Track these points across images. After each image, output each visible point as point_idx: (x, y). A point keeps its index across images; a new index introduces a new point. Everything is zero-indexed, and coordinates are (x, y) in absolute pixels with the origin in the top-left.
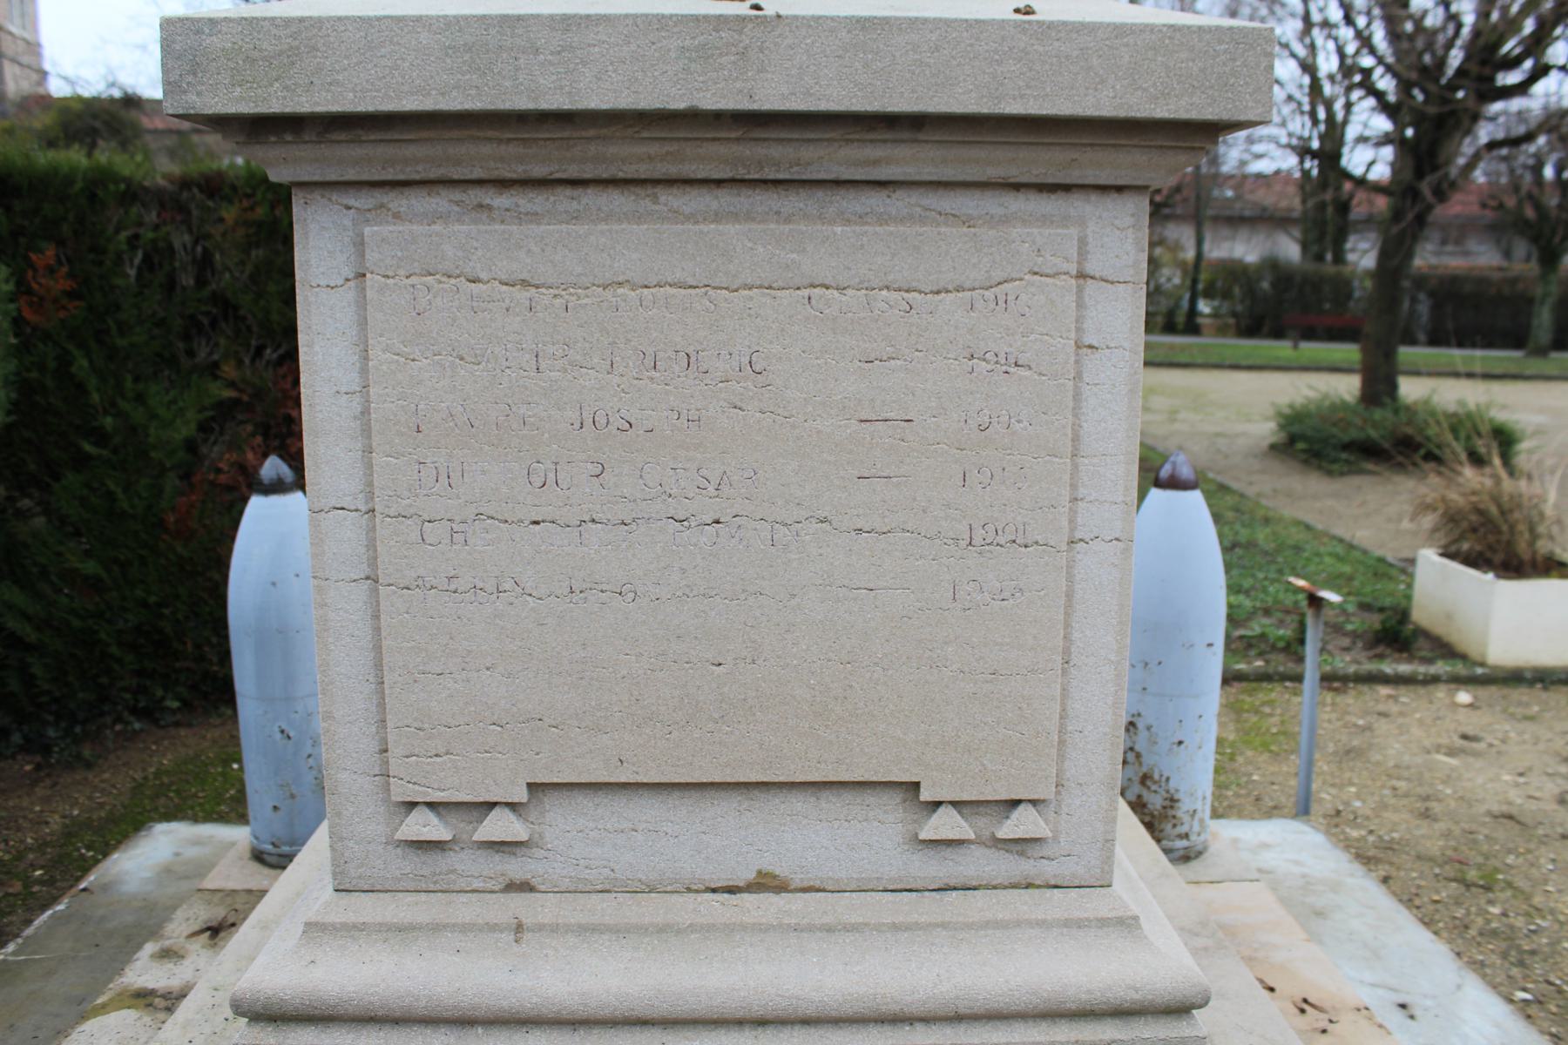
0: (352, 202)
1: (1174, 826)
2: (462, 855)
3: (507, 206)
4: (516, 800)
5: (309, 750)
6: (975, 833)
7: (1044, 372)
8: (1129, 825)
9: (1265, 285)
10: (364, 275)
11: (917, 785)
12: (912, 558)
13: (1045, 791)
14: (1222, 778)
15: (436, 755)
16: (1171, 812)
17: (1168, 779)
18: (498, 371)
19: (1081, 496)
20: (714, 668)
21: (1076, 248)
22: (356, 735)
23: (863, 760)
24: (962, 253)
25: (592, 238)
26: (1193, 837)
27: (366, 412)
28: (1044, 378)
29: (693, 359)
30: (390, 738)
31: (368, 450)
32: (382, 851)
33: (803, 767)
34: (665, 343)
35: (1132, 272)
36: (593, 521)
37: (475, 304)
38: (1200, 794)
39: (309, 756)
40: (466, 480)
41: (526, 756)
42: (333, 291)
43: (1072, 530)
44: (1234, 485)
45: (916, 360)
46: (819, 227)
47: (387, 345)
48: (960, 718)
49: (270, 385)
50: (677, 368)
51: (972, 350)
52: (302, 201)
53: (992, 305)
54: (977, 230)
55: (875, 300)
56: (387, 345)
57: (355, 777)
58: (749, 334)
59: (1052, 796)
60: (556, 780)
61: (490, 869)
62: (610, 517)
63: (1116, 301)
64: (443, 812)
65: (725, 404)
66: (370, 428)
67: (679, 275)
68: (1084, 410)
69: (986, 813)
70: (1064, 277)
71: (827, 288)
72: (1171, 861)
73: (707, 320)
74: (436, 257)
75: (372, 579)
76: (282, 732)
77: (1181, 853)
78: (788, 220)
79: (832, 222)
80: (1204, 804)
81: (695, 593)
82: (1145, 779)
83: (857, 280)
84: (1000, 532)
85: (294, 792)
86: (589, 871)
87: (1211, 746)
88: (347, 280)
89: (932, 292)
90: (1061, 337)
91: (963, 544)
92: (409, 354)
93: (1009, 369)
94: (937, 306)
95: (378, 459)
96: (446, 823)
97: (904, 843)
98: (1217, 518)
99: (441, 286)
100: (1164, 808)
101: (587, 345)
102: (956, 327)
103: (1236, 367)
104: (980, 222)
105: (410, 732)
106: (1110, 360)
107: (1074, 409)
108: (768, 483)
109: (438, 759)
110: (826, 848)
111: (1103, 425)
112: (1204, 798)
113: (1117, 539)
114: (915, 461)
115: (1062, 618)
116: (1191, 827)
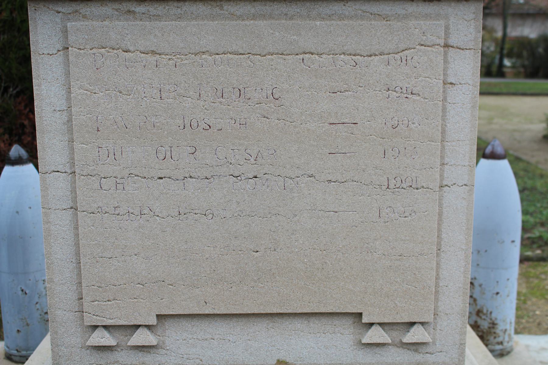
0: (60, 9)
1: (495, 338)
2: (122, 353)
3: (144, 12)
4: (151, 324)
5: (37, 300)
6: (391, 340)
7: (427, 97)
8: (472, 337)
9: (541, 50)
10: (68, 48)
11: (360, 314)
12: (357, 195)
13: (428, 318)
14: (520, 313)
15: (108, 301)
16: (493, 331)
17: (491, 313)
18: (140, 99)
19: (446, 162)
20: (254, 253)
21: (443, 31)
22: (66, 291)
23: (332, 301)
24: (383, 35)
25: (189, 28)
26: (505, 344)
27: (70, 120)
28: (426, 100)
29: (242, 92)
30: (84, 292)
31: (71, 141)
32: (79, 352)
33: (301, 305)
34: (227, 84)
35: (473, 43)
36: (191, 177)
37: (127, 64)
38: (508, 321)
39: (37, 303)
40: (123, 156)
41: (156, 300)
42: (51, 57)
43: (442, 180)
44: (524, 157)
45: (359, 92)
46: (308, 22)
47: (81, 85)
48: (383, 279)
49: (13, 107)
50: (234, 97)
51: (388, 86)
52: (33, 8)
53: (399, 62)
54: (391, 22)
55: (337, 60)
56: (81, 85)
57: (65, 313)
58: (272, 79)
59: (432, 320)
60: (171, 313)
61: (137, 360)
62: (199, 175)
63: (465, 59)
64: (112, 331)
65: (259, 116)
66: (72, 129)
67: (234, 48)
68: (448, 117)
69: (397, 329)
70: (437, 47)
71: (312, 54)
72: (495, 356)
73: (249, 71)
74: (106, 38)
75: (74, 208)
76: (22, 290)
77: (498, 352)
78: (291, 18)
79: (315, 19)
80: (511, 326)
81: (244, 214)
82: (479, 313)
83: (328, 50)
84: (403, 182)
85: (29, 322)
86: (189, 361)
87: (514, 295)
88: (59, 51)
89: (367, 56)
90: (436, 78)
91: (384, 188)
92: (93, 90)
93: (408, 96)
94: (370, 63)
95: (77, 146)
96: (114, 336)
97: (354, 345)
98: (516, 174)
99: (109, 54)
100: (489, 328)
101: (187, 85)
102: (380, 74)
103: (524, 94)
104: (393, 18)
105: (94, 289)
106: (461, 90)
107: (442, 116)
108: (282, 156)
109: (109, 303)
110: (313, 348)
111: (458, 124)
112: (511, 323)
113: (465, 185)
114: (358, 145)
115: (436, 226)
116: (504, 338)
